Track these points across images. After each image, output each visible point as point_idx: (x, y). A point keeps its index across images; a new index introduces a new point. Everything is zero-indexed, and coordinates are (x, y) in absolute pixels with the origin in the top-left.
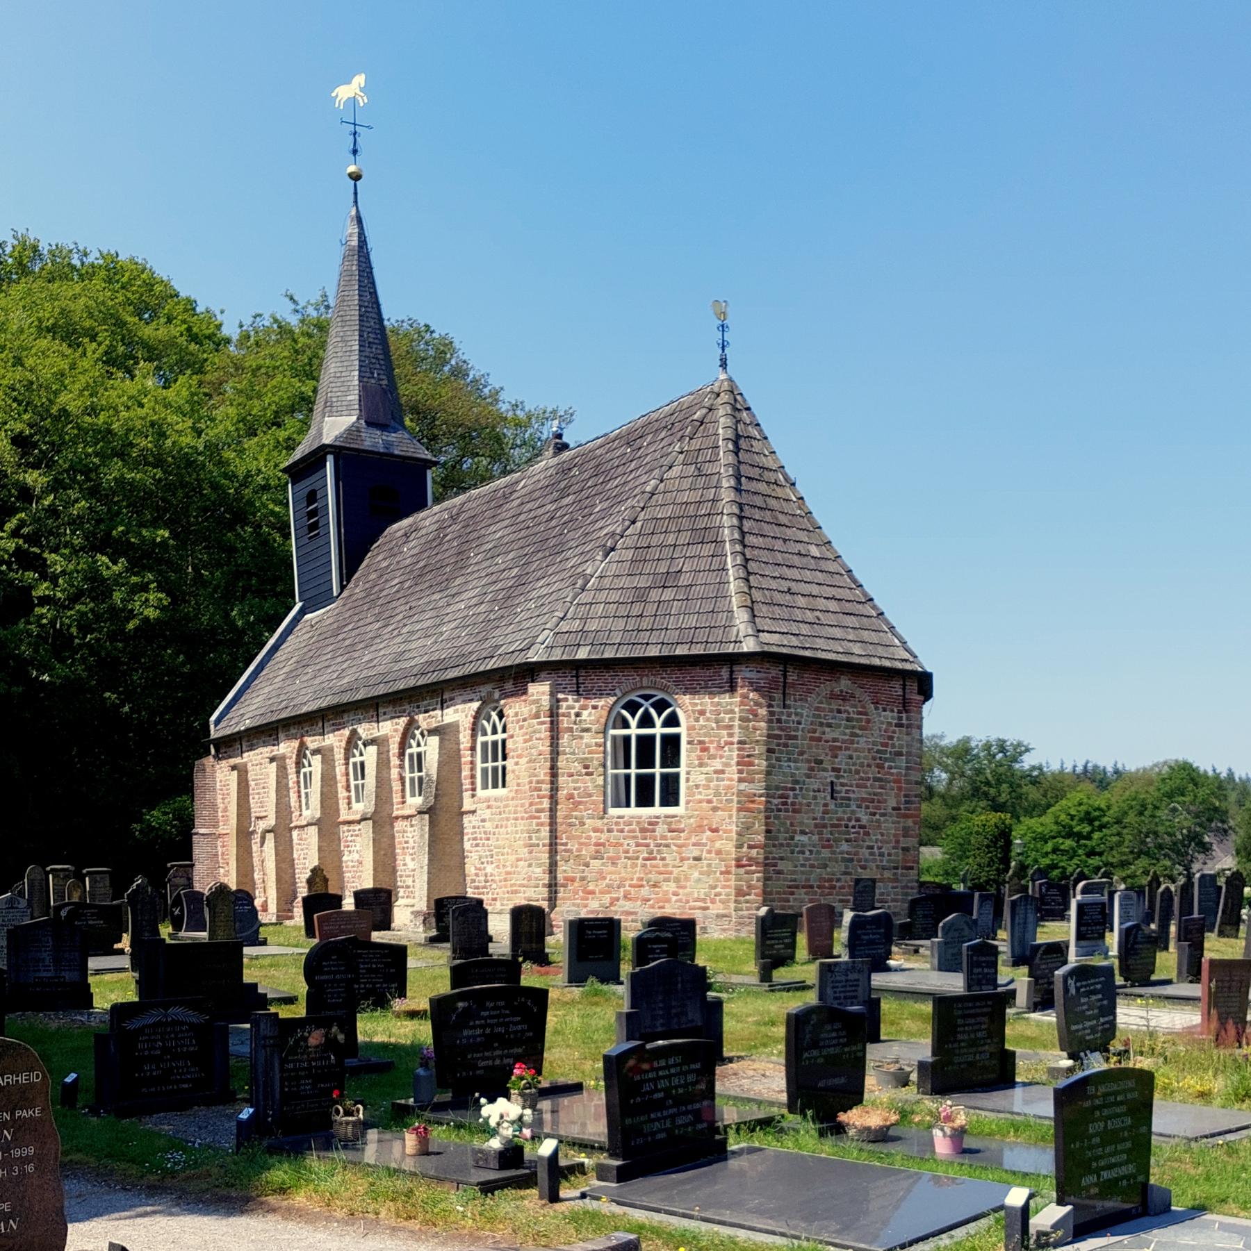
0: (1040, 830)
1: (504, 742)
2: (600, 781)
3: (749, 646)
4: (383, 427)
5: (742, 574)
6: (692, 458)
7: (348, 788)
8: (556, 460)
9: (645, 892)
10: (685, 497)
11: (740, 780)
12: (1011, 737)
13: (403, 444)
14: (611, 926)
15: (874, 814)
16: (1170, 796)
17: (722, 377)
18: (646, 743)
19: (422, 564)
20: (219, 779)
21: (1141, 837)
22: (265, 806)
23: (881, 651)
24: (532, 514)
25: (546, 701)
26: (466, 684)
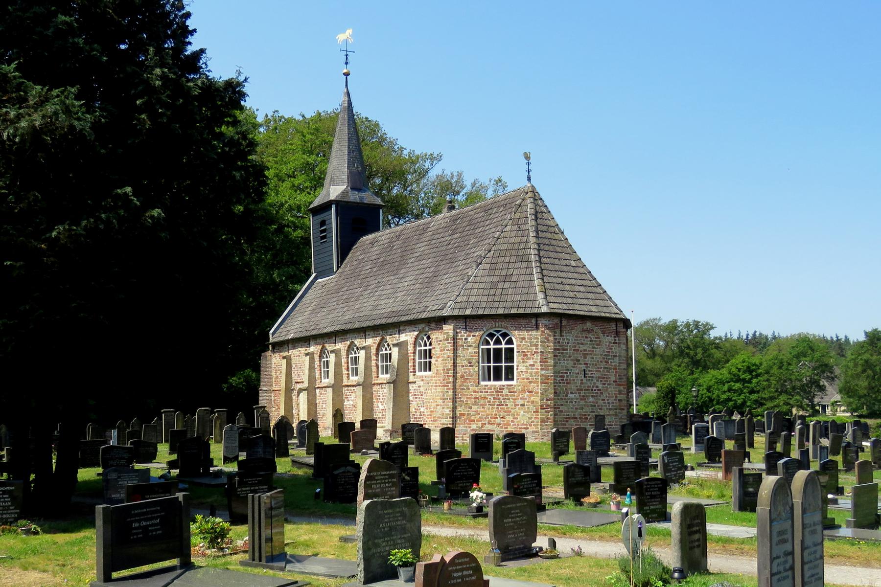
0: (720, 377)
1: (430, 350)
2: (476, 369)
3: (544, 309)
4: (359, 190)
5: (540, 276)
6: (516, 223)
7: (348, 369)
8: (449, 214)
9: (498, 420)
10: (512, 240)
11: (542, 369)
12: (702, 320)
13: (369, 197)
14: (489, 437)
16: (797, 356)
17: (529, 185)
18: (498, 352)
19: (382, 260)
20: (274, 364)
21: (782, 382)
22: (302, 375)
23: (605, 309)
24: (439, 241)
25: (451, 333)
26: (412, 323)
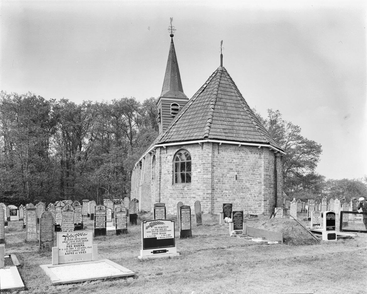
15: (252, 184)
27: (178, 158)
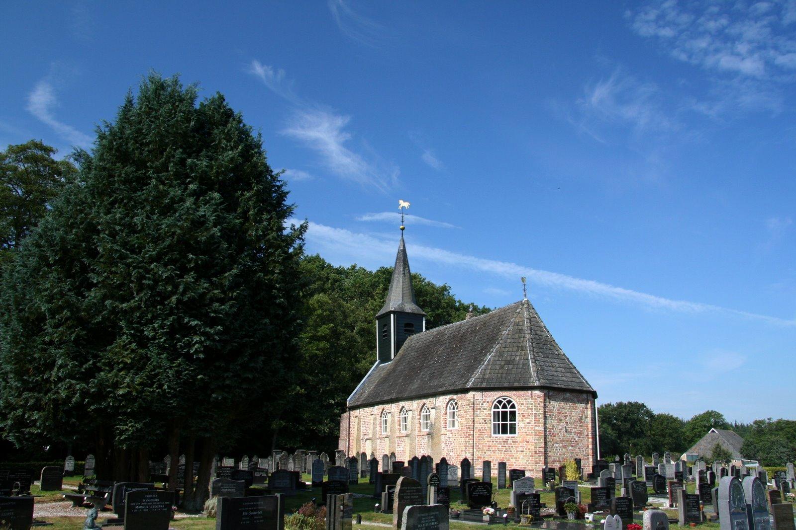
15: (580, 437)
27: (511, 405)
